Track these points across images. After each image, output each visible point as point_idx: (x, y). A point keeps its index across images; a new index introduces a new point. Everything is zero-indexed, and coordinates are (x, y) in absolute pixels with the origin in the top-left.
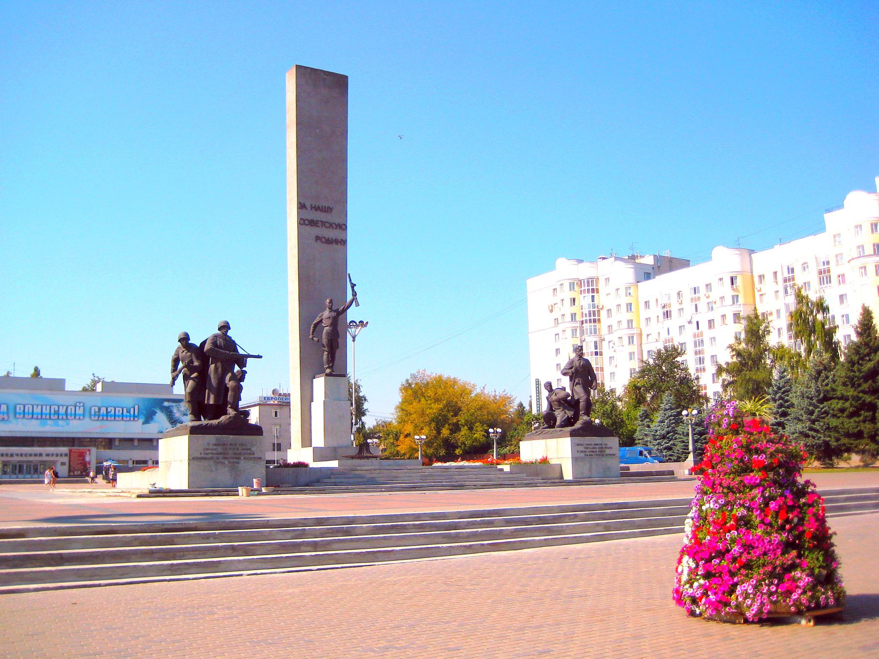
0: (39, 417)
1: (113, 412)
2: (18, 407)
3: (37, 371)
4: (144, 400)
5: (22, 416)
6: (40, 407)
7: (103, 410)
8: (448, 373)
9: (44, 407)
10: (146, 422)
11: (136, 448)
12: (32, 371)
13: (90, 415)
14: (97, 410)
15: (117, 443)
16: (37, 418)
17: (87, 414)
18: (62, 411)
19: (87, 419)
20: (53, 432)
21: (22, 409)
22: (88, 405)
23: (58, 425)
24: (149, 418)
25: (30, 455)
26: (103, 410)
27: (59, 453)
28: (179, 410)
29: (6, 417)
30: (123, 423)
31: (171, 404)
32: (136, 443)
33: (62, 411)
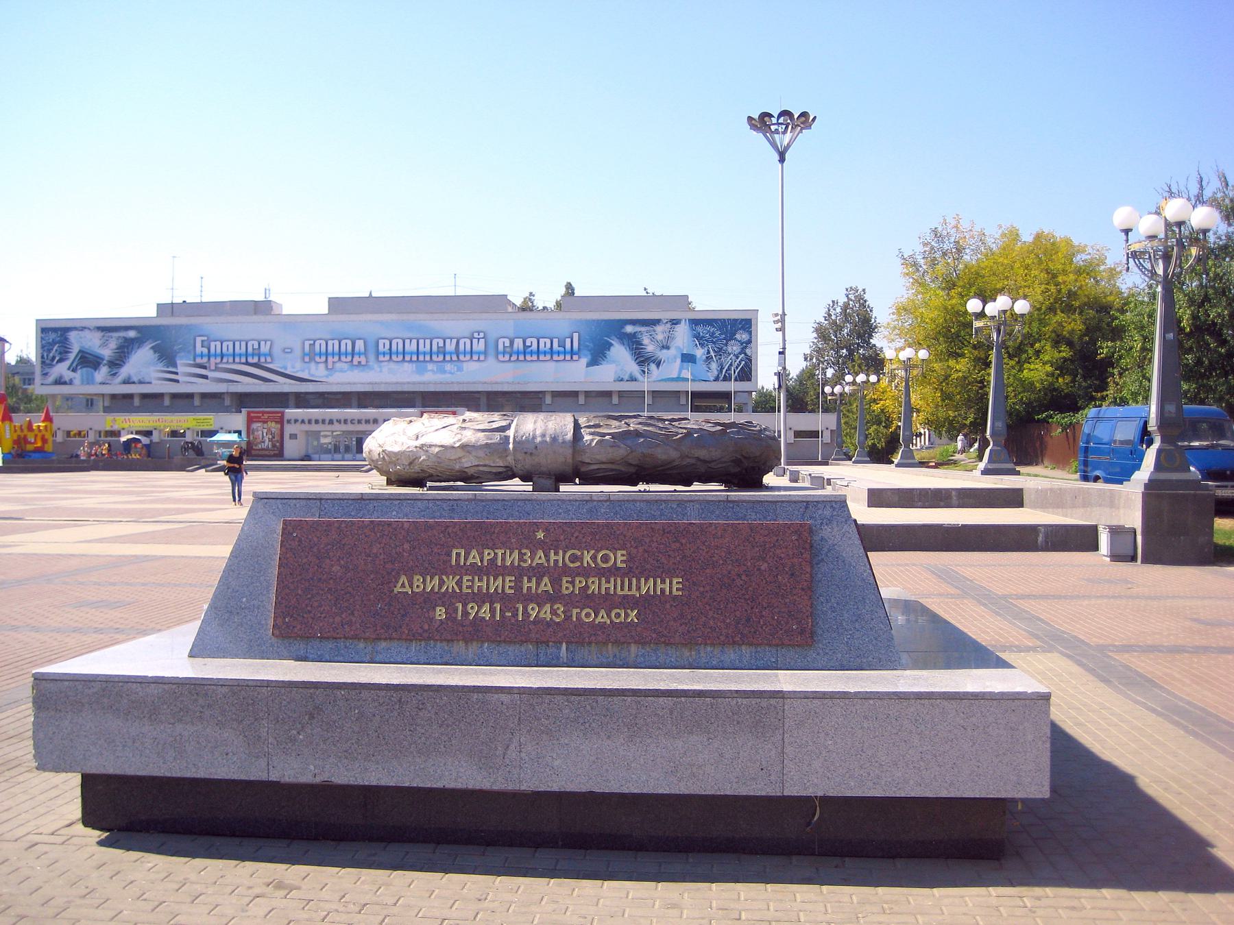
0: (414, 358)
1: (535, 347)
2: (381, 342)
3: (570, 288)
4: (589, 322)
5: (387, 357)
6: (414, 342)
7: (518, 344)
8: (1059, 230)
9: (421, 342)
10: (594, 362)
11: (193, 410)
12: (563, 291)
13: (497, 353)
14: (507, 344)
15: (548, 400)
16: (411, 361)
17: (491, 351)
18: (450, 347)
19: (491, 360)
20: (414, 383)
21: (387, 346)
22: (492, 336)
23: (445, 372)
24: (598, 354)
25: (359, 422)
26: (518, 344)
27: (320, 419)
28: (653, 339)
29: (363, 359)
30: (553, 364)
31: (638, 329)
32: (197, 402)
33: (450, 347)
